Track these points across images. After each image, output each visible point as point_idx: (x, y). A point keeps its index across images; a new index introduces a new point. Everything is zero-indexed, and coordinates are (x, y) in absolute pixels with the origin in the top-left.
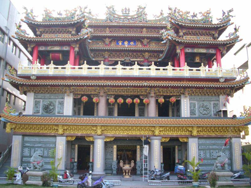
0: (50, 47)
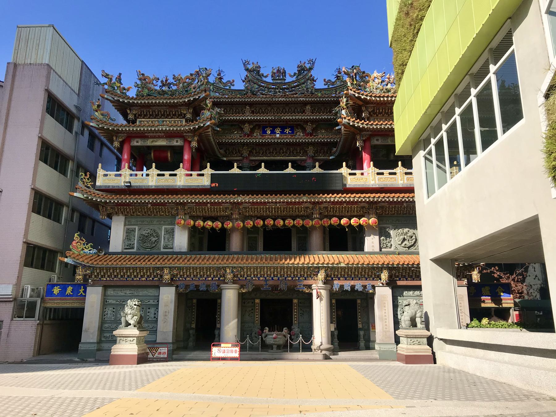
0: (152, 140)
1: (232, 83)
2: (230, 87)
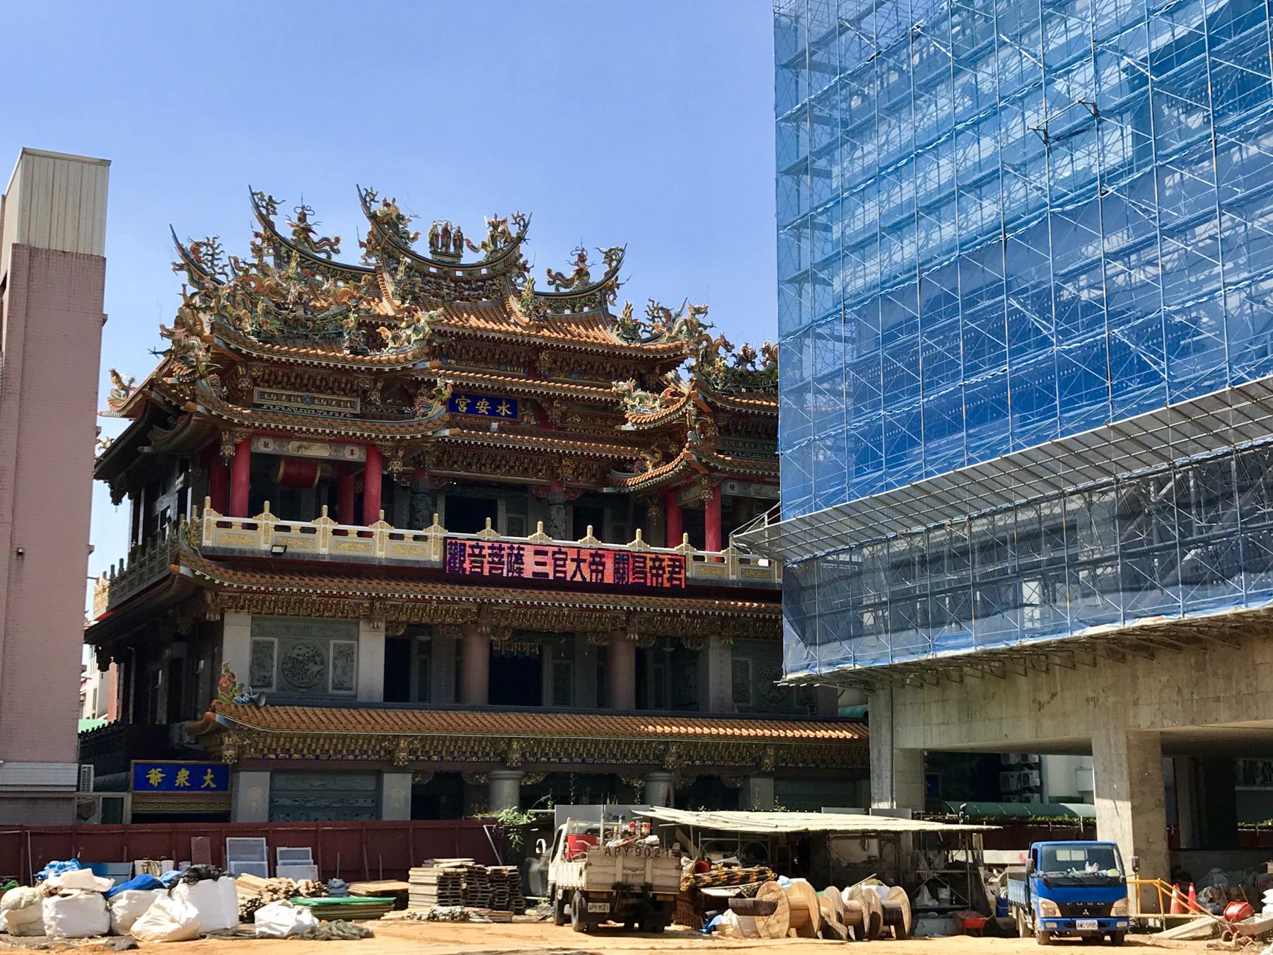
0: (297, 444)
1: (332, 244)
2: (329, 257)
